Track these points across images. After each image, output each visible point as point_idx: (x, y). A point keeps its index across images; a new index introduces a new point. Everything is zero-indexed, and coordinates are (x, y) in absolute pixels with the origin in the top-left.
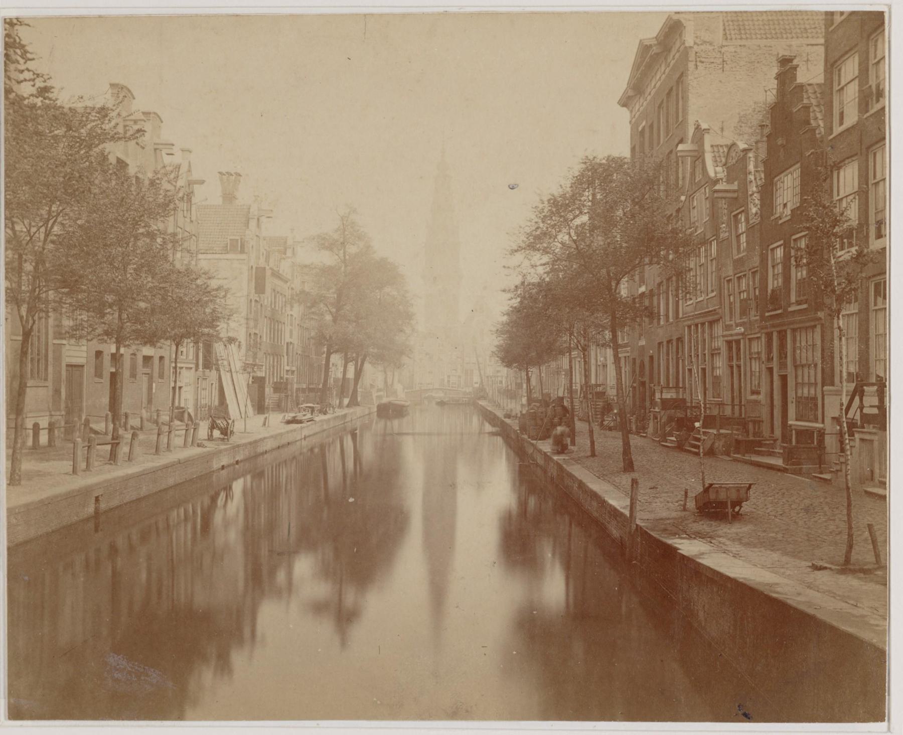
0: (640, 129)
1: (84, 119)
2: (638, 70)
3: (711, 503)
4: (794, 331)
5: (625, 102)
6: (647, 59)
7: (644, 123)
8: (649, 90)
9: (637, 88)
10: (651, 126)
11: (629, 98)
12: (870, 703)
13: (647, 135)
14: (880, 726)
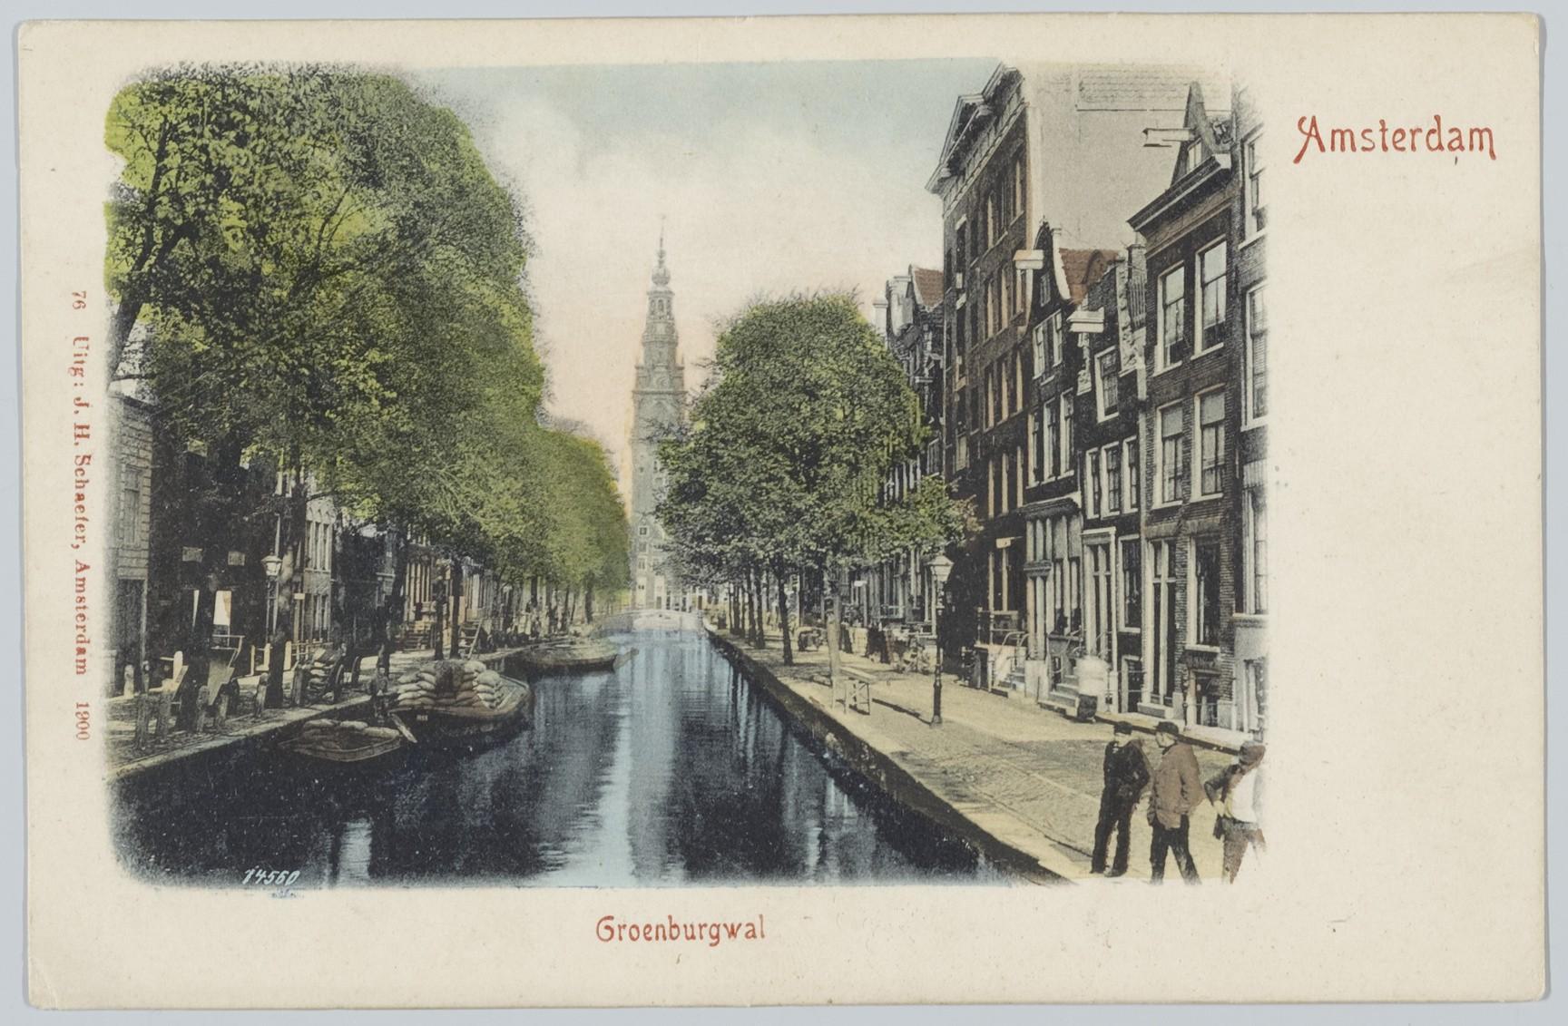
3: (733, 574)
4: (1164, 412)
5: (939, 187)
7: (964, 218)
9: (956, 166)
10: (975, 307)
11: (942, 180)
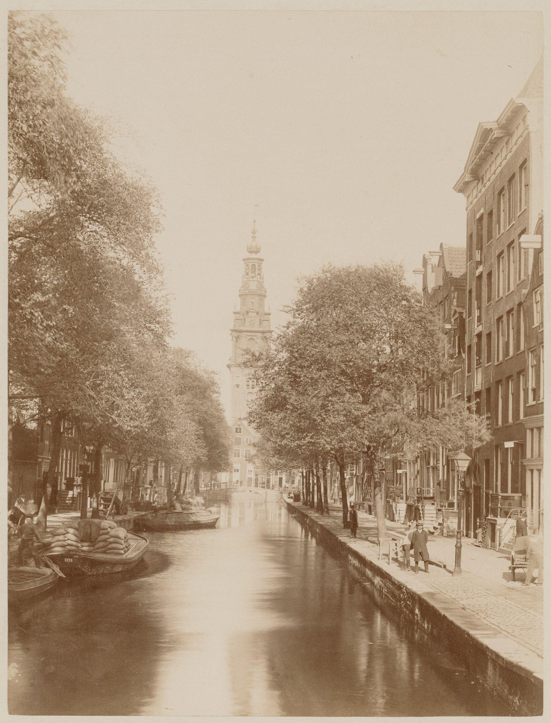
0: (478, 216)
1: (300, 389)
2: (477, 154)
6: (487, 144)
8: (488, 176)
9: (476, 173)
10: (490, 214)
11: (467, 183)
12: (536, 709)
13: (485, 222)
14: (7, 712)
